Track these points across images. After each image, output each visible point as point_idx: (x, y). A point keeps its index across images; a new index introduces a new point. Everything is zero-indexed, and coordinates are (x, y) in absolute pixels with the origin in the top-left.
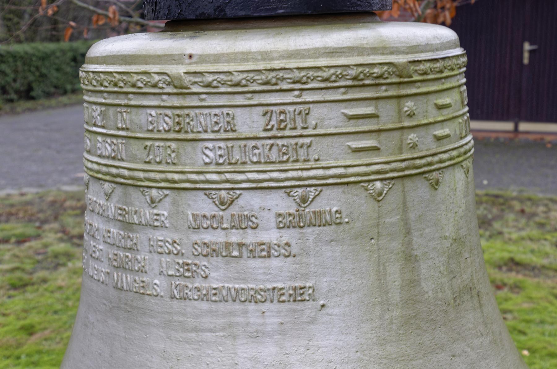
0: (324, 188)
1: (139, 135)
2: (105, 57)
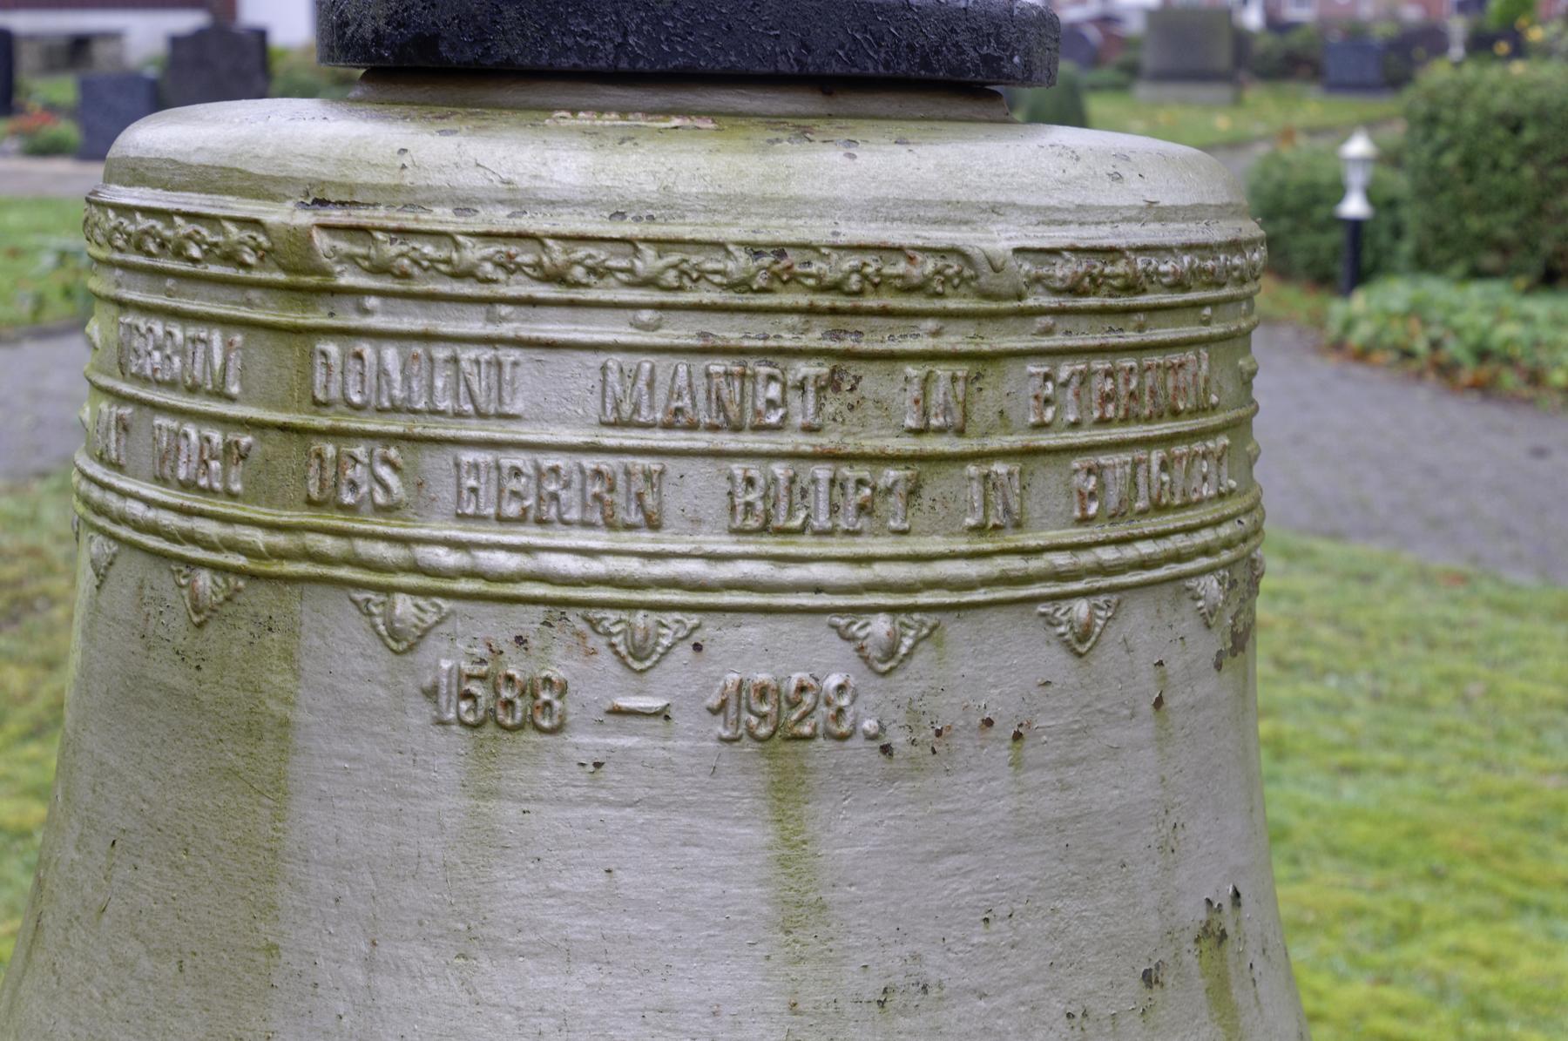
0: (947, 619)
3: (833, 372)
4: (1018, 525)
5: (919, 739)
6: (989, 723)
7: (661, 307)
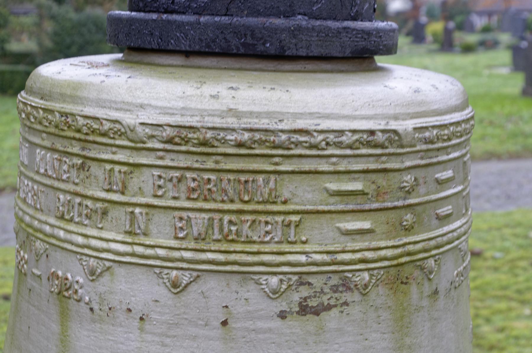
3: (83, 163)
4: (145, 234)
5: (103, 309)
6: (129, 310)
7: (282, 156)
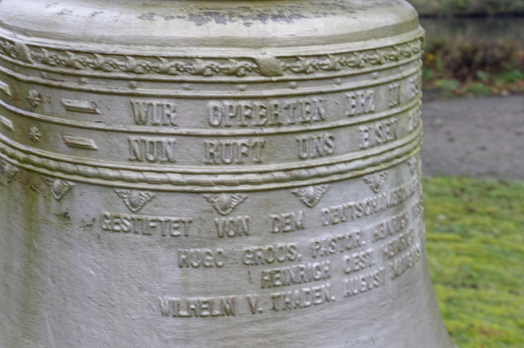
1: (341, 123)
2: (372, 30)
